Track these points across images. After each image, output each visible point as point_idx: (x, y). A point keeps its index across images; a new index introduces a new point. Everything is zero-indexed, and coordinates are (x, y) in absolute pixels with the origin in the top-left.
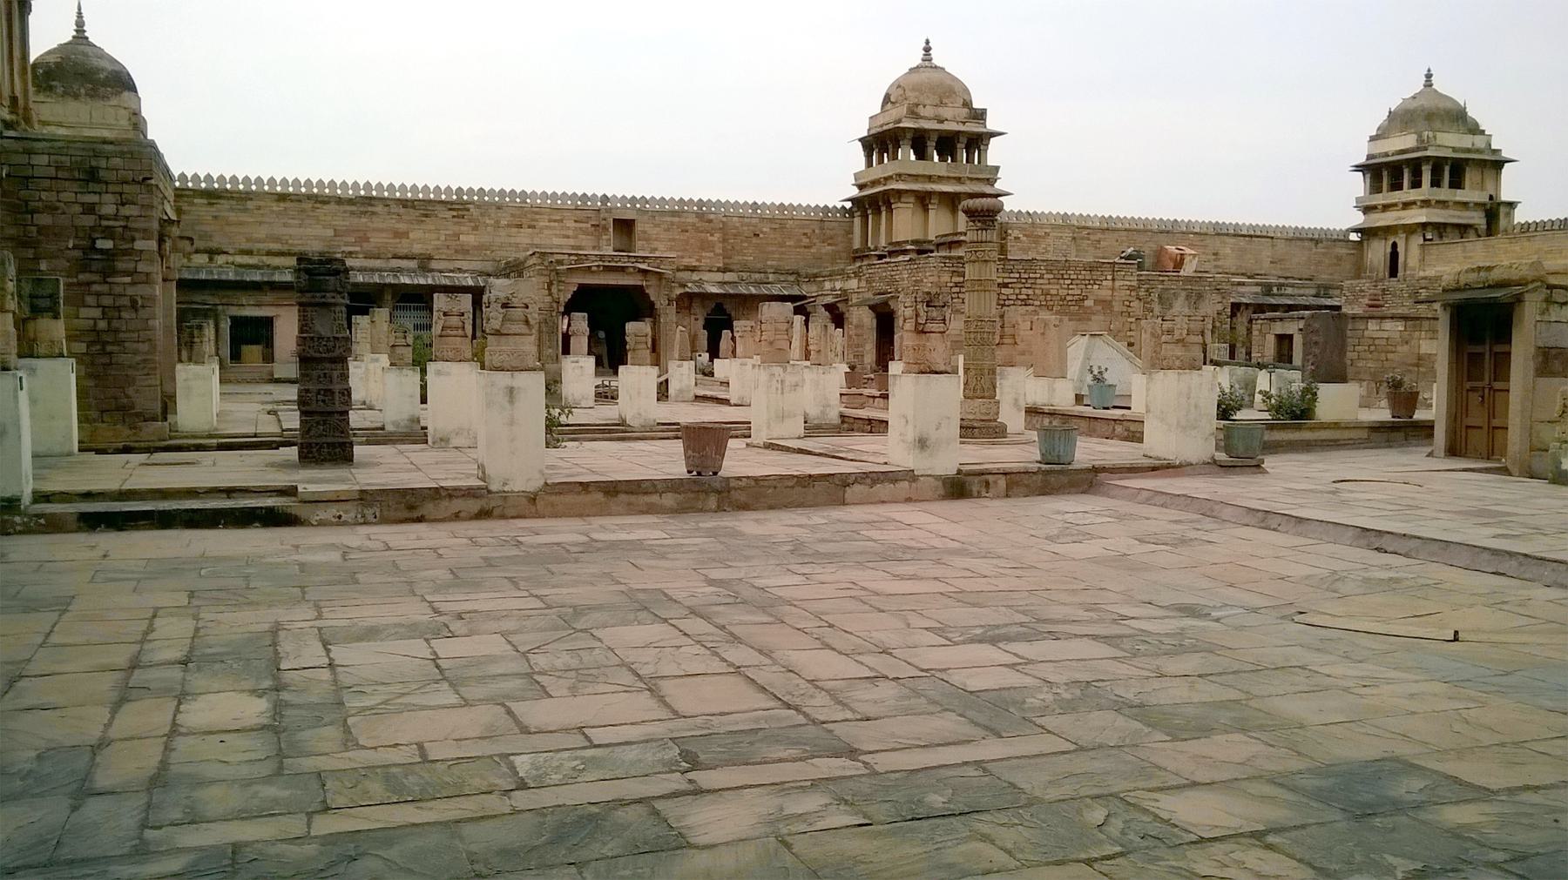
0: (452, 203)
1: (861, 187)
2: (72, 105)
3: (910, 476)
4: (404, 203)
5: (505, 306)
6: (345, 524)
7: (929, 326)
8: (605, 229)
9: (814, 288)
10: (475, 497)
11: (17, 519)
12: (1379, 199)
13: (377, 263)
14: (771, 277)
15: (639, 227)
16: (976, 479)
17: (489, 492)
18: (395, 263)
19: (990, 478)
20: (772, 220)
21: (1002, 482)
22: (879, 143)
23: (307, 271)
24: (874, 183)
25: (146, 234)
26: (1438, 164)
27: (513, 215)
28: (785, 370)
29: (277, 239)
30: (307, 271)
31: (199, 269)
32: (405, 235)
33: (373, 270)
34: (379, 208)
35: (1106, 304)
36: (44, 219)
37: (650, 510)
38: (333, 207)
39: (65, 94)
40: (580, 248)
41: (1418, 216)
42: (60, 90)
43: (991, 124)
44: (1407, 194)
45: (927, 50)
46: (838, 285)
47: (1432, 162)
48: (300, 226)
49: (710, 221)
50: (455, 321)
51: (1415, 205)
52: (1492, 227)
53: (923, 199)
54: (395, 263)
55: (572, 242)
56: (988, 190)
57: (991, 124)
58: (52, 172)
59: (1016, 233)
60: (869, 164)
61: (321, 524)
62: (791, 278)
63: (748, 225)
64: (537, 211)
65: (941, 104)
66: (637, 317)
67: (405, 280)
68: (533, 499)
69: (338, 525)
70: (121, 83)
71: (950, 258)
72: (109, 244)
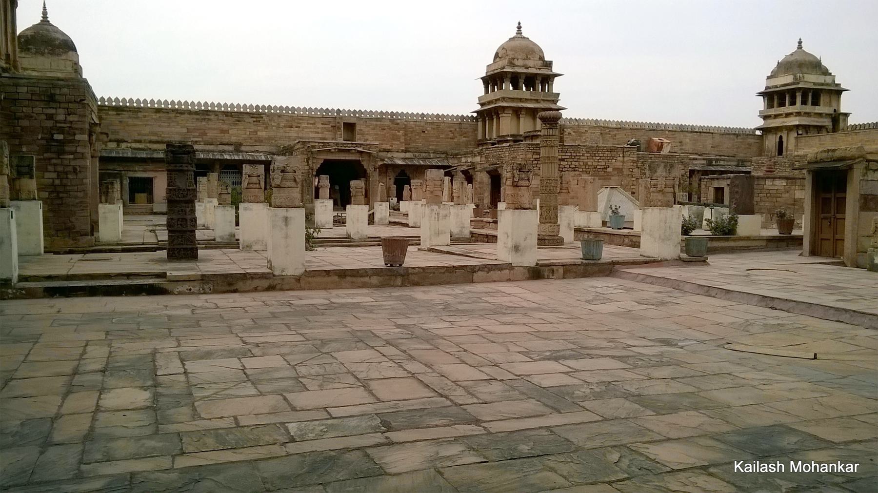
0: (253, 114)
1: (482, 105)
2: (40, 59)
3: (510, 267)
4: (226, 114)
5: (283, 171)
6: (193, 293)
8: (339, 128)
10: (266, 278)
11: (10, 291)
12: (772, 112)
13: (211, 147)
14: (432, 155)
15: (358, 127)
16: (547, 269)
19: (554, 268)
21: (561, 270)
22: (492, 80)
23: (172, 152)
24: (490, 103)
26: (805, 92)
28: (439, 207)
29: (155, 134)
30: (172, 152)
31: (111, 150)
32: (227, 131)
33: (209, 151)
34: (212, 117)
35: (619, 170)
36: (25, 123)
38: (186, 116)
39: (36, 53)
40: (325, 139)
41: (794, 121)
42: (34, 50)
43: (555, 70)
44: (788, 109)
45: (519, 28)
46: (469, 160)
47: (802, 90)
48: (168, 126)
49: (398, 124)
50: (255, 180)
51: (792, 116)
52: (835, 128)
53: (517, 112)
55: (320, 135)
56: (553, 106)
58: (29, 96)
59: (569, 131)
60: (487, 92)
61: (180, 293)
62: (443, 156)
63: (419, 126)
64: (301, 118)
65: (527, 58)
67: (227, 157)
68: (298, 279)
69: (189, 294)
70: (68, 46)
71: (532, 144)
72: (61, 137)
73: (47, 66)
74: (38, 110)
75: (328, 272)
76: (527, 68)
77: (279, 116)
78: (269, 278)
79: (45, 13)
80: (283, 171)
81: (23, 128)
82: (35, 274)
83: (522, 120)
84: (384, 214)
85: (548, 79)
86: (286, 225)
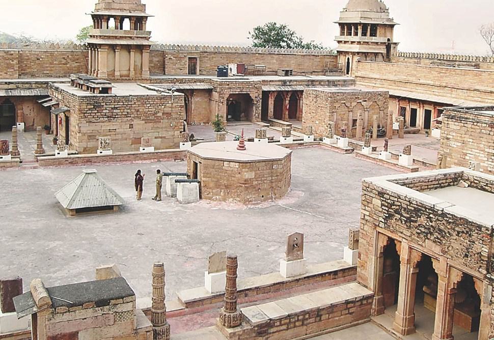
12: (343, 38)
26: (365, 26)
35: (168, 114)
41: (356, 48)
43: (148, 12)
44: (353, 38)
51: (355, 44)
52: (387, 57)
56: (145, 43)
59: (169, 56)
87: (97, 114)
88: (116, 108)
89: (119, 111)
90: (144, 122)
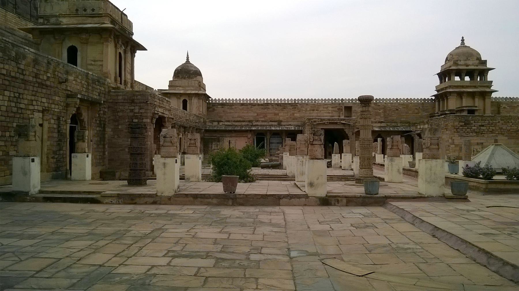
0: (293, 104)
1: (438, 91)
2: (184, 81)
3: (306, 196)
4: (278, 104)
5: (164, 137)
6: (113, 204)
7: (315, 142)
8: (342, 110)
9: (414, 128)
10: (152, 197)
11: (28, 198)
13: (265, 123)
14: (399, 124)
15: (353, 109)
16: (333, 199)
17: (157, 196)
18: (271, 123)
19: (339, 199)
20: (403, 104)
21: (345, 200)
22: (443, 75)
23: (131, 128)
24: (442, 89)
25: (147, 117)
27: (311, 107)
28: (303, 157)
29: (241, 117)
30: (131, 128)
31: (215, 126)
32: (278, 114)
33: (264, 126)
34: (270, 107)
36: (120, 114)
37: (208, 204)
38: (257, 107)
39: (182, 78)
40: (333, 116)
42: (181, 77)
43: (489, 66)
45: (463, 40)
46: (422, 127)
47: (465, 71)
48: (247, 113)
49: (379, 106)
50: (193, 142)
53: (460, 95)
54: (271, 123)
55: (330, 115)
56: (488, 90)
57: (489, 66)
58: (123, 101)
59: (504, 105)
60: (441, 82)
61: (107, 203)
62: (407, 125)
63: (394, 106)
64: (319, 105)
65: (467, 59)
66: (344, 139)
67: (273, 128)
68: (169, 198)
69: (111, 204)
70: (197, 73)
71: (460, 116)
72: (136, 121)
73: (187, 84)
74: (127, 107)
75: (187, 195)
76: (467, 66)
77: (307, 104)
78: (153, 197)
79: (188, 58)
80: (164, 137)
81: (119, 117)
82: (264, 192)
83: (464, 100)
84: (337, 161)
85: (484, 73)
86: (164, 167)
87: (467, 130)
88: (483, 126)
89: (485, 128)
90: (507, 138)
